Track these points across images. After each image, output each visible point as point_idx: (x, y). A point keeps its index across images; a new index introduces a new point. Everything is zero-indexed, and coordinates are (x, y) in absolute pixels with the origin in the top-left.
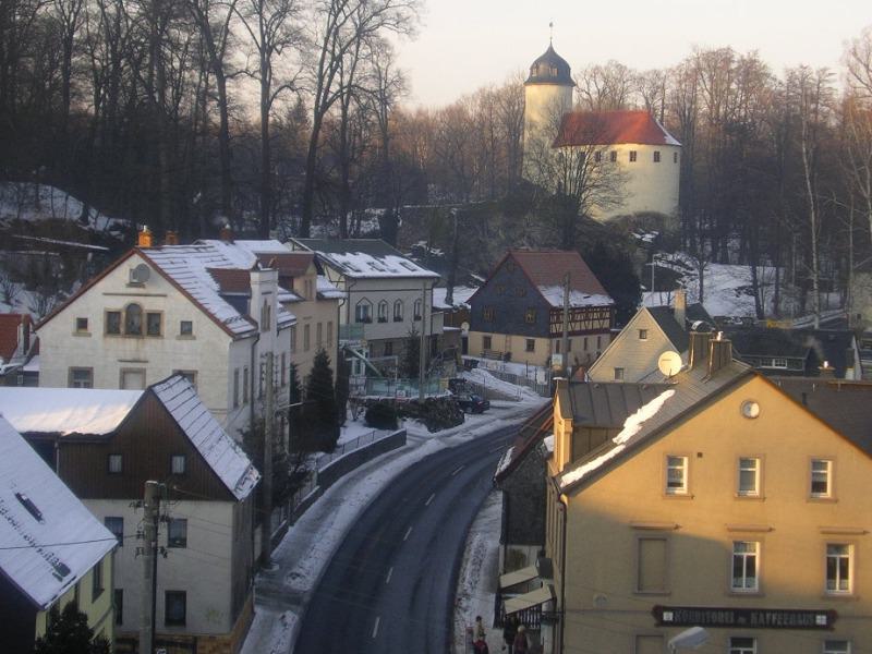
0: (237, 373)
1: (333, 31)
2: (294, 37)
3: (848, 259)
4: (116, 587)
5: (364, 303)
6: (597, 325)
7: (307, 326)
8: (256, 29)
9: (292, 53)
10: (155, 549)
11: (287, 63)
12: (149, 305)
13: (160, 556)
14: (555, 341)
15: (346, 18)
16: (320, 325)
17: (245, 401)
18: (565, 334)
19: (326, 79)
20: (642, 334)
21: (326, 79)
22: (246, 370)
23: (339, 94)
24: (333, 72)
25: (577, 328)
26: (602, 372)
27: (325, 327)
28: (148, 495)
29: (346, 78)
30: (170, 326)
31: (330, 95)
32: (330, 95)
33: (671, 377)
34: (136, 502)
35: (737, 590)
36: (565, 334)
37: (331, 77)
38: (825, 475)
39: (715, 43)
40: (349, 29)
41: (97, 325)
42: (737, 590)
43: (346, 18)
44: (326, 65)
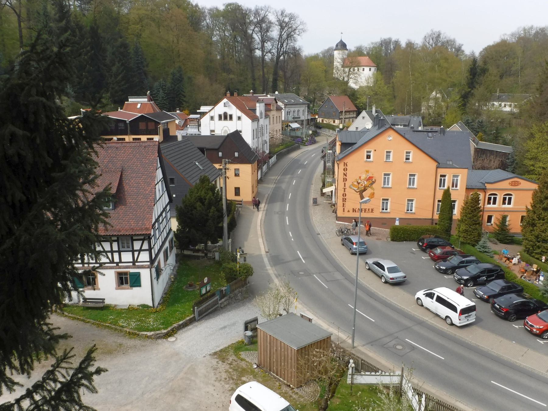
0: (254, 130)
1: (281, 36)
2: (271, 39)
3: (462, 265)
4: (221, 186)
5: (289, 111)
6: (352, 116)
7: (273, 117)
8: (260, 37)
9: (269, 43)
10: (226, 177)
11: (268, 45)
12: (229, 113)
13: (227, 179)
14: (341, 120)
15: (284, 32)
16: (277, 117)
17: (256, 138)
18: (343, 119)
19: (279, 50)
20: (363, 117)
21: (279, 50)
22: (256, 129)
23: (283, 54)
24: (281, 48)
25: (347, 117)
26: (352, 128)
27: (278, 117)
28: (223, 163)
29: (285, 50)
30: (235, 118)
31: (280, 54)
32: (280, 54)
33: (368, 129)
34: (220, 164)
35: (410, 186)
36: (343, 119)
37: (281, 49)
38: (409, 156)
39: (386, 36)
40: (285, 36)
41: (216, 118)
42: (410, 186)
43: (284, 32)
44: (279, 46)
